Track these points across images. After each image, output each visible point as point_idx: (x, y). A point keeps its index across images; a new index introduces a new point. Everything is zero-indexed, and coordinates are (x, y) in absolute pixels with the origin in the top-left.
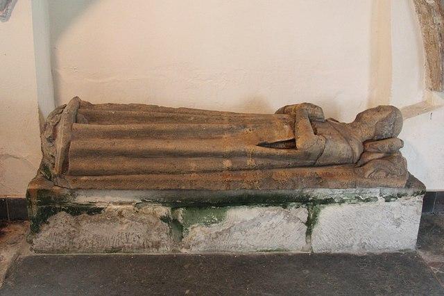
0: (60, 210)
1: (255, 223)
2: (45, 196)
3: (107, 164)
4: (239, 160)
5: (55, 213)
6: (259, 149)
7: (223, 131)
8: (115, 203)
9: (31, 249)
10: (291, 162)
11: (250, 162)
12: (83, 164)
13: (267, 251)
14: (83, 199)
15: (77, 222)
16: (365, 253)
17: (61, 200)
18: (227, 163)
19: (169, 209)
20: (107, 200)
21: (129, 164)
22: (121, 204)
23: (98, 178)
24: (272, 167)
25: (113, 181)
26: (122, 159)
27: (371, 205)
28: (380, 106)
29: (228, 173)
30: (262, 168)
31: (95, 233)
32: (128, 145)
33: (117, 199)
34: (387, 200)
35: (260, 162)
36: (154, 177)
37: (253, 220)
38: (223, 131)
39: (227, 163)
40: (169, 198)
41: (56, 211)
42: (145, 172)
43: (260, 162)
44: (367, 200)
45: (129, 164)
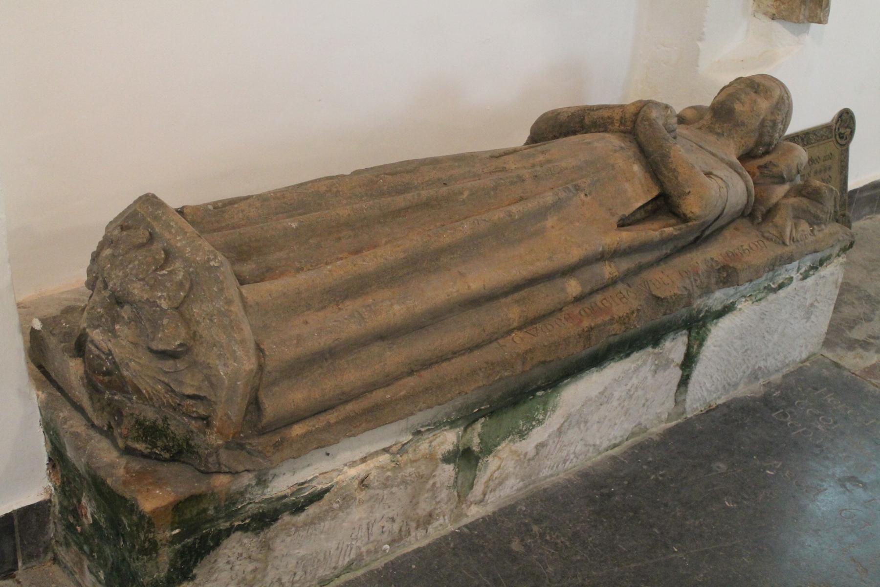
0: (228, 532)
1: (604, 397)
2: (190, 513)
3: (351, 375)
4: (586, 273)
5: (217, 544)
6: (627, 236)
7: (542, 213)
8: (353, 464)
9: (834, 475)
10: (666, 250)
11: (608, 270)
12: (297, 396)
13: (615, 446)
14: (282, 484)
15: (267, 547)
16: (756, 388)
17: (230, 504)
18: (573, 287)
19: (460, 430)
20: (343, 463)
21: (393, 357)
22: (364, 460)
23: (332, 417)
24: (640, 269)
25: (353, 411)
26: (375, 349)
27: (789, 289)
28: (139, 229)
29: (576, 310)
30: (625, 277)
31: (302, 552)
32: (392, 308)
33: (358, 455)
34: (805, 277)
35: (625, 265)
36: (449, 368)
37: (601, 393)
38: (542, 213)
39: (573, 287)
40: (459, 410)
41: (219, 538)
42: (427, 364)
43: (625, 265)
44: (781, 286)
45: (393, 357)
